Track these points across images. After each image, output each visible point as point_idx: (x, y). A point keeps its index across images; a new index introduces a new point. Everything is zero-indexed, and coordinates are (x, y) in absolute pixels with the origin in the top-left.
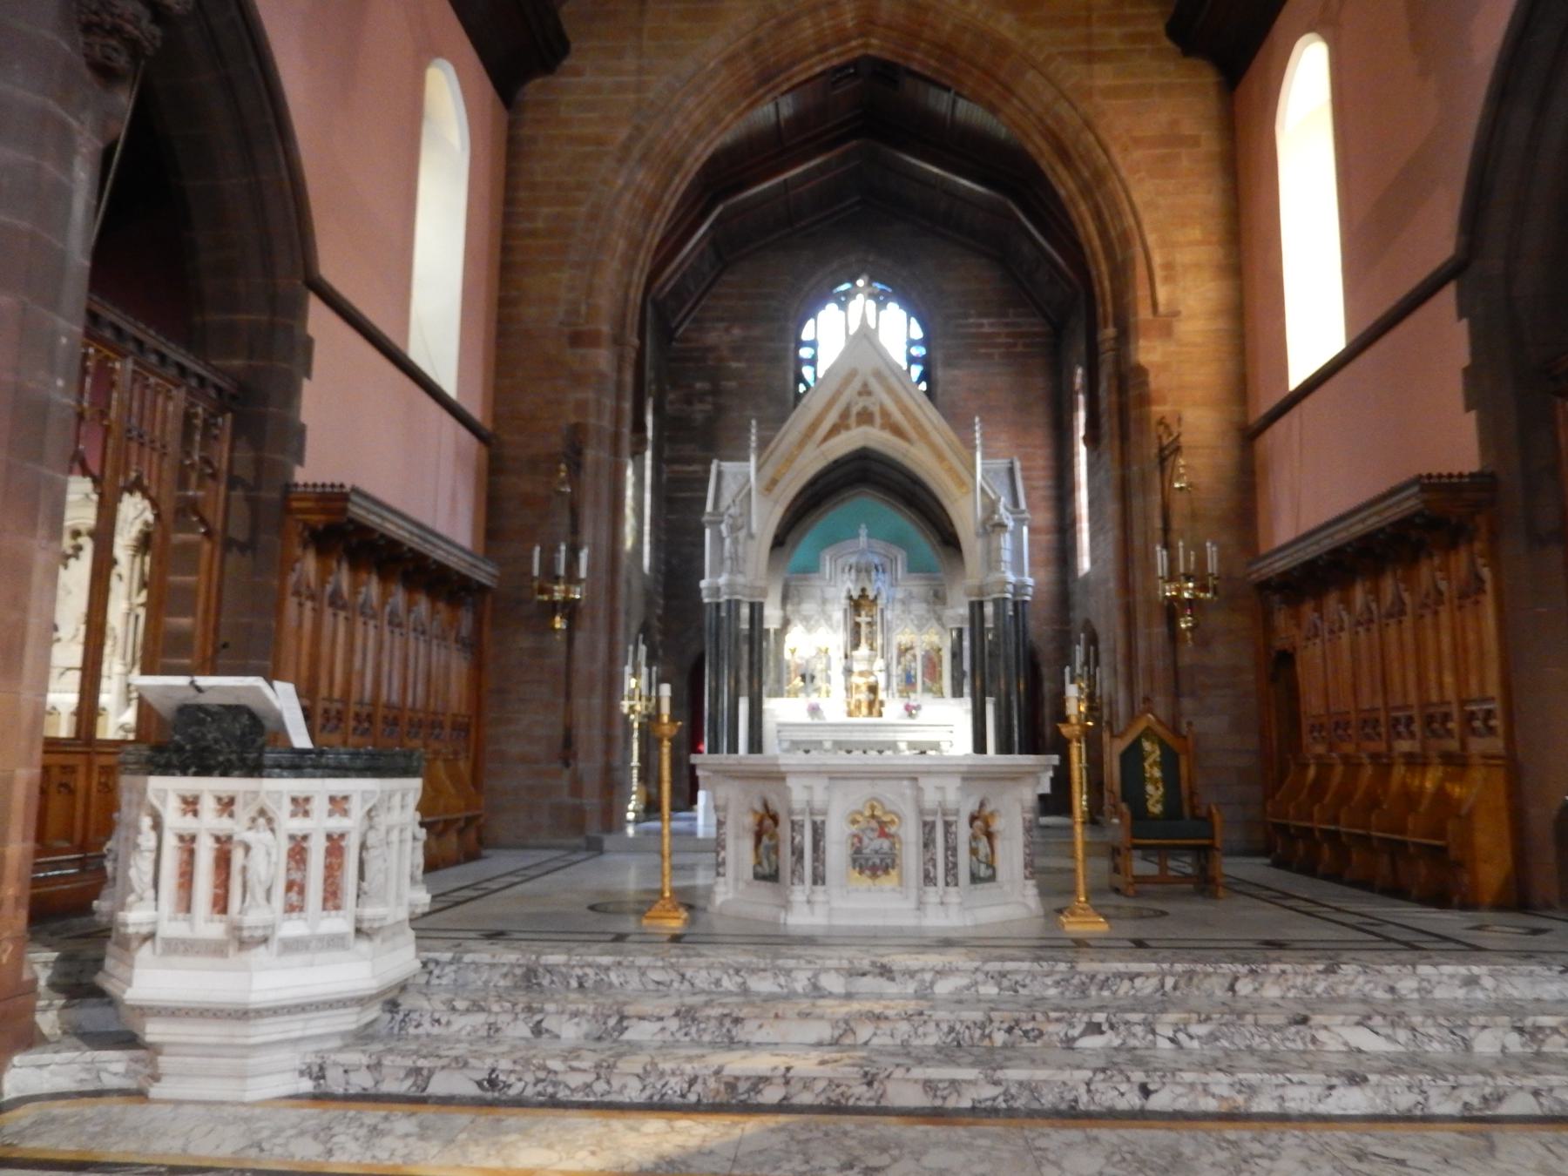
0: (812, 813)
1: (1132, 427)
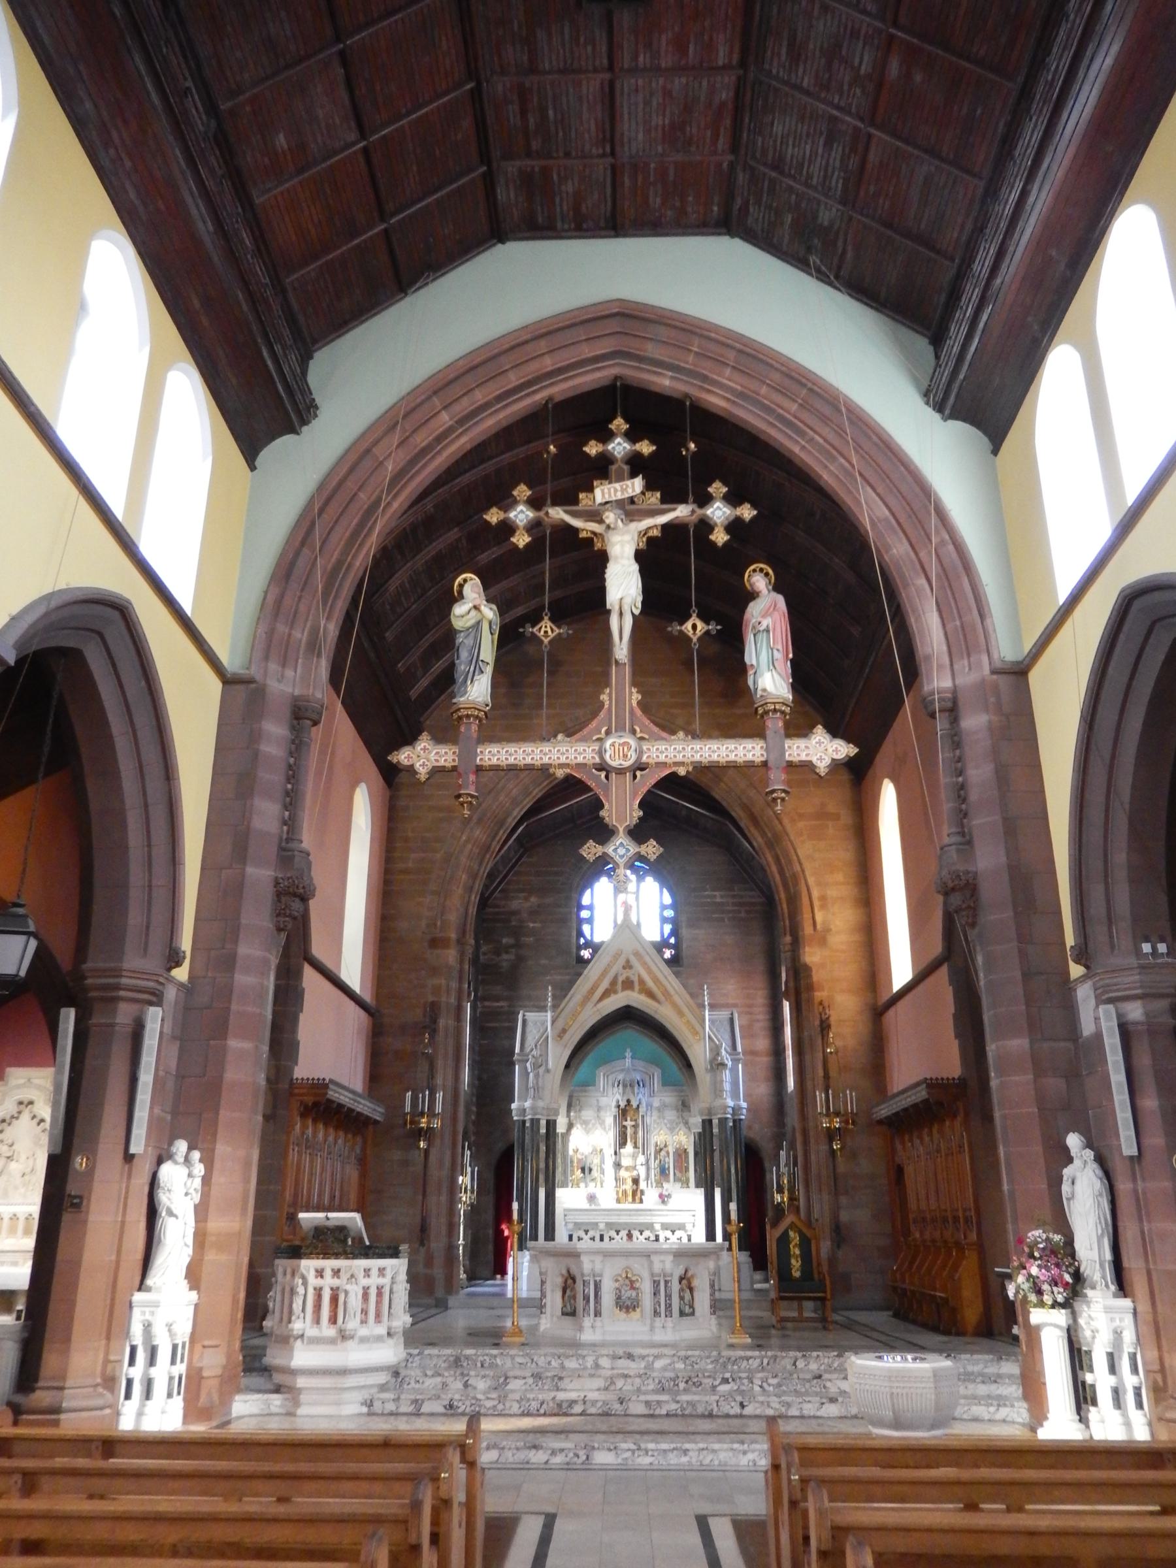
0: (594, 1276)
1: (804, 1007)
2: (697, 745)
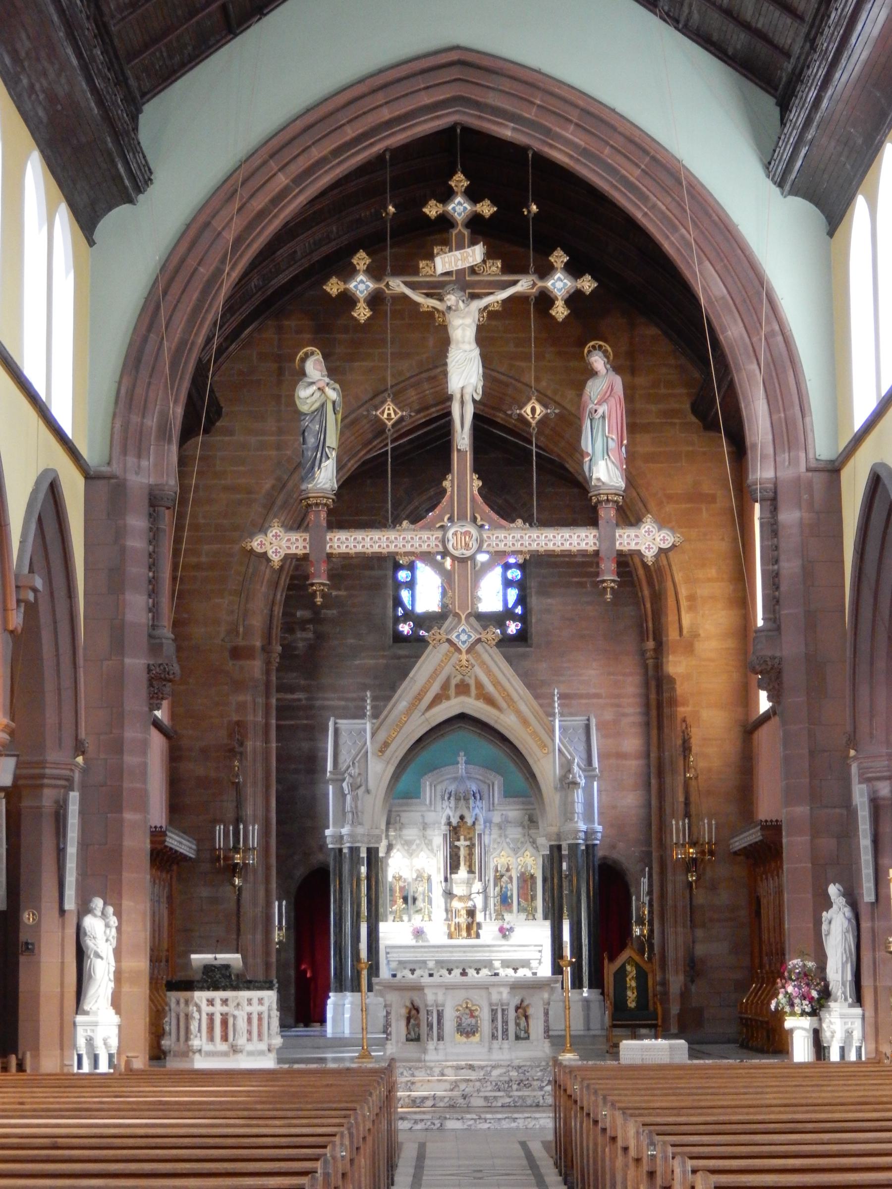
0: (437, 1006)
2: (534, 533)
